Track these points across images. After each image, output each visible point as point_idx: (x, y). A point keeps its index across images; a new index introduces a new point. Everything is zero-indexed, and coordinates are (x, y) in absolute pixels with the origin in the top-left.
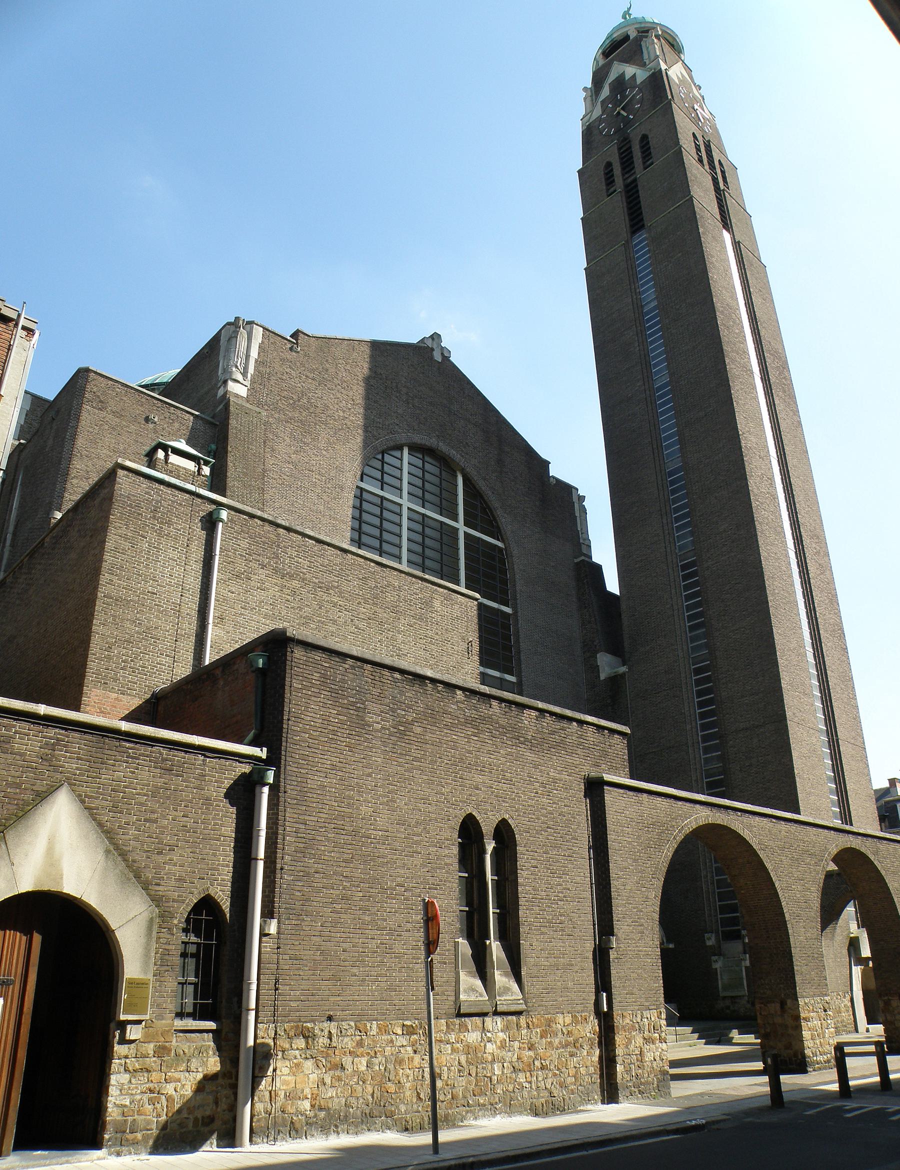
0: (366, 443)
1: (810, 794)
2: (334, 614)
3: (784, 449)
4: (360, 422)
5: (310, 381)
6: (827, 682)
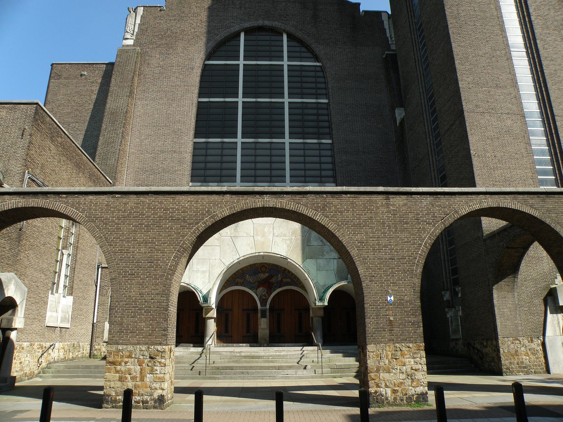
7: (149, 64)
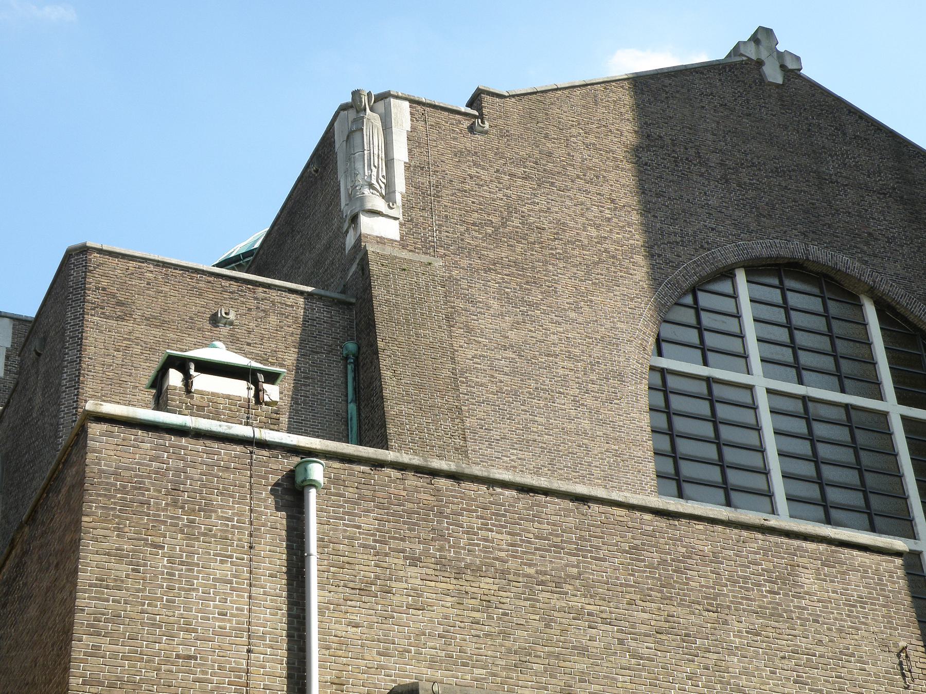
0: (657, 278)
2: (579, 634)
4: (637, 239)
5: (520, 182)
7: (469, 330)
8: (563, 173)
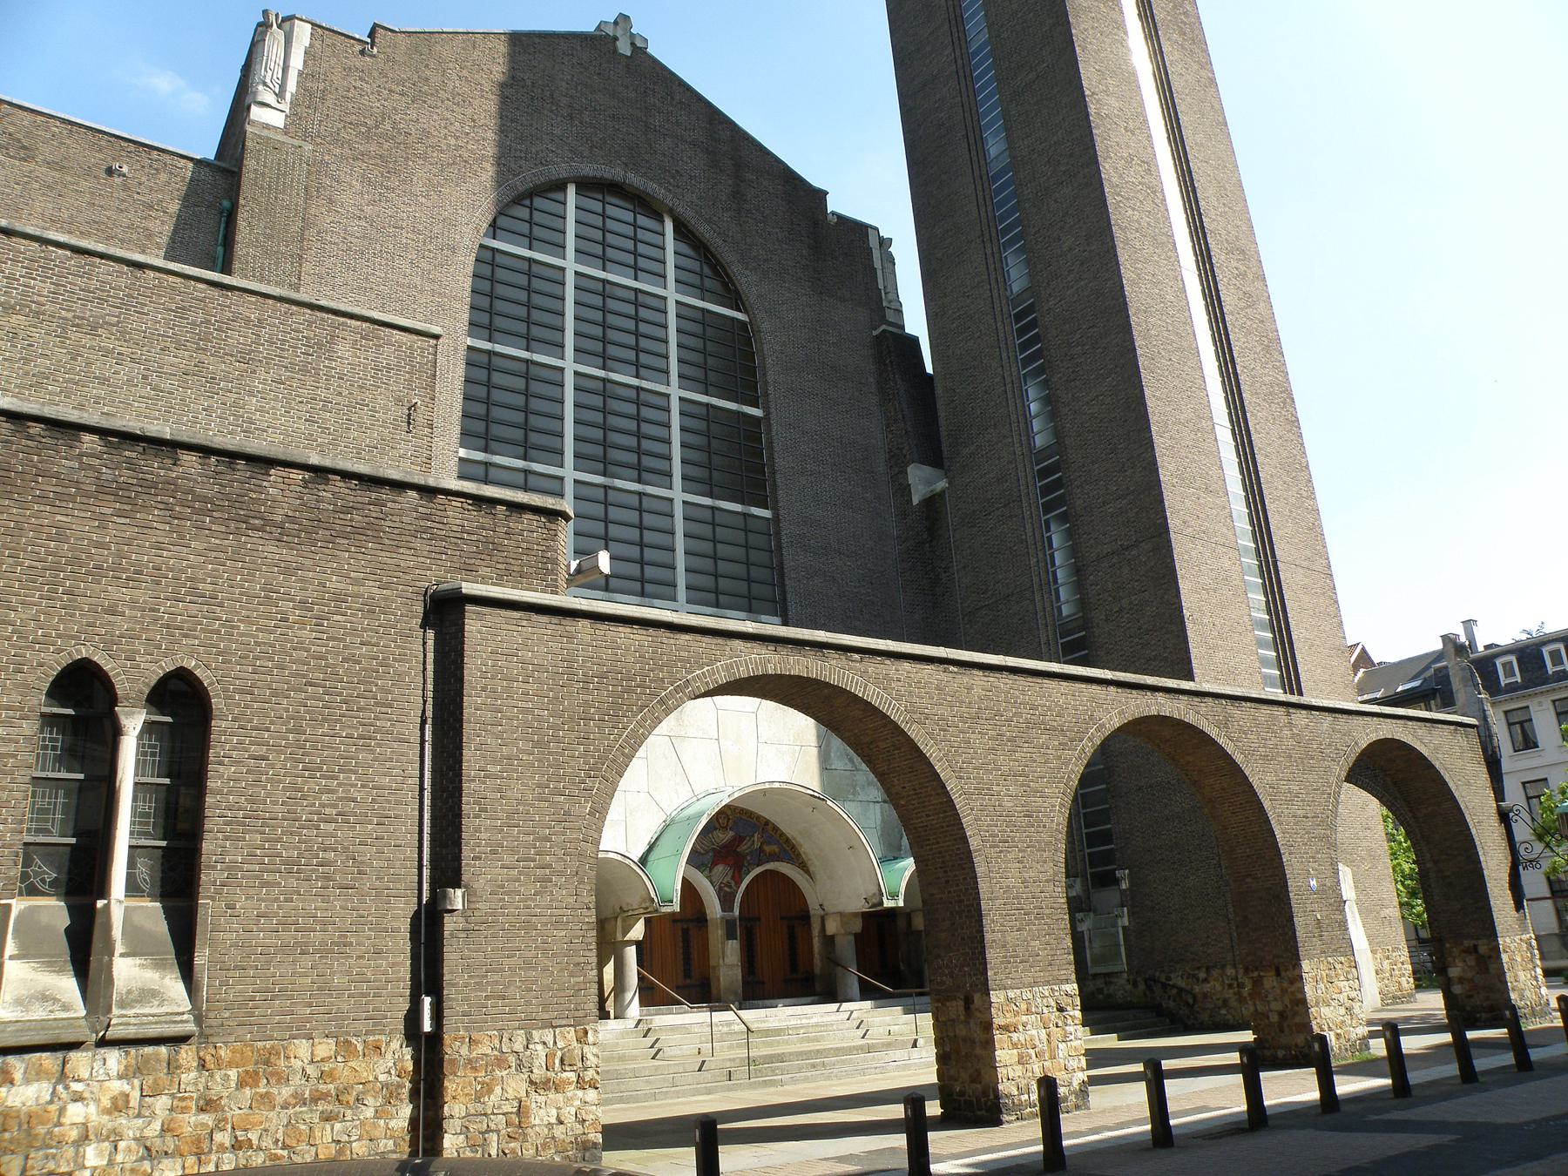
1: (1215, 648)
3: (1178, 119)
4: (490, 151)
5: (397, 97)
6: (1257, 472)
7: (331, 201)
8: (435, 94)
